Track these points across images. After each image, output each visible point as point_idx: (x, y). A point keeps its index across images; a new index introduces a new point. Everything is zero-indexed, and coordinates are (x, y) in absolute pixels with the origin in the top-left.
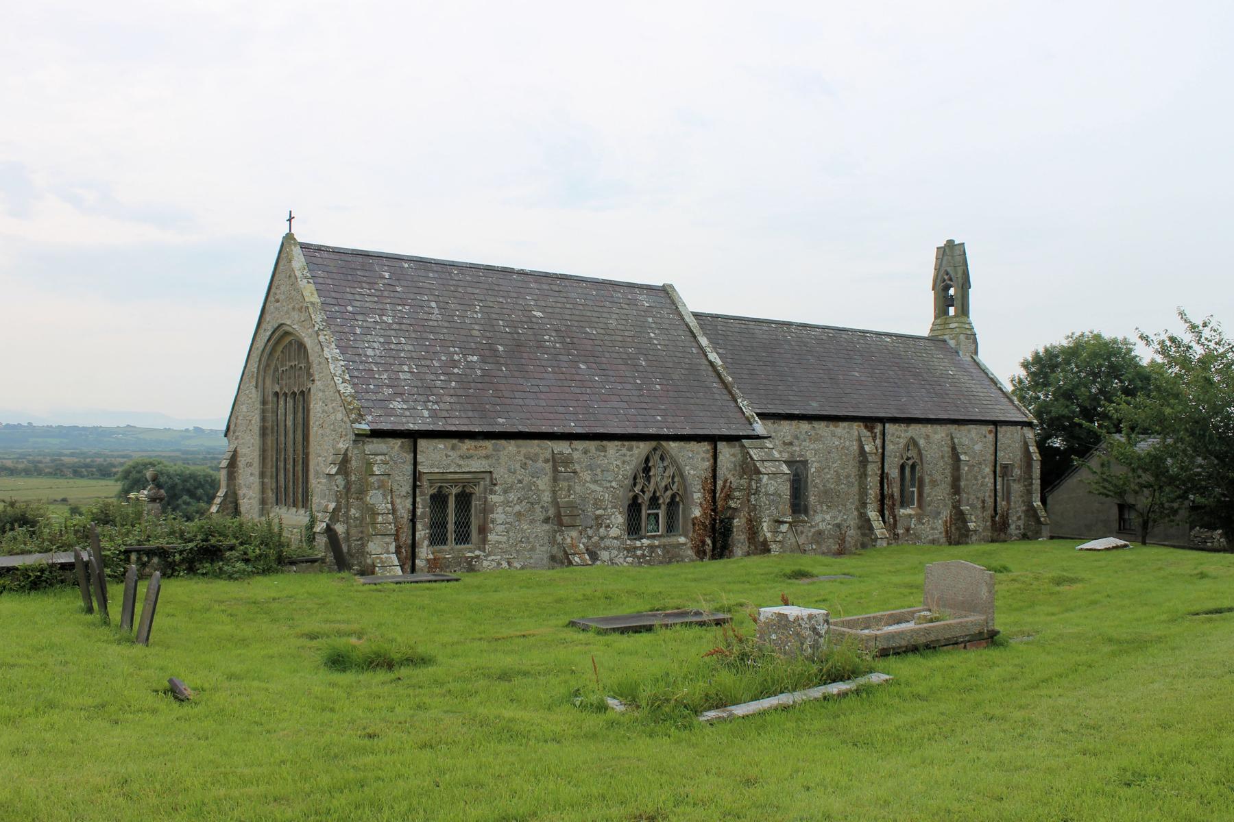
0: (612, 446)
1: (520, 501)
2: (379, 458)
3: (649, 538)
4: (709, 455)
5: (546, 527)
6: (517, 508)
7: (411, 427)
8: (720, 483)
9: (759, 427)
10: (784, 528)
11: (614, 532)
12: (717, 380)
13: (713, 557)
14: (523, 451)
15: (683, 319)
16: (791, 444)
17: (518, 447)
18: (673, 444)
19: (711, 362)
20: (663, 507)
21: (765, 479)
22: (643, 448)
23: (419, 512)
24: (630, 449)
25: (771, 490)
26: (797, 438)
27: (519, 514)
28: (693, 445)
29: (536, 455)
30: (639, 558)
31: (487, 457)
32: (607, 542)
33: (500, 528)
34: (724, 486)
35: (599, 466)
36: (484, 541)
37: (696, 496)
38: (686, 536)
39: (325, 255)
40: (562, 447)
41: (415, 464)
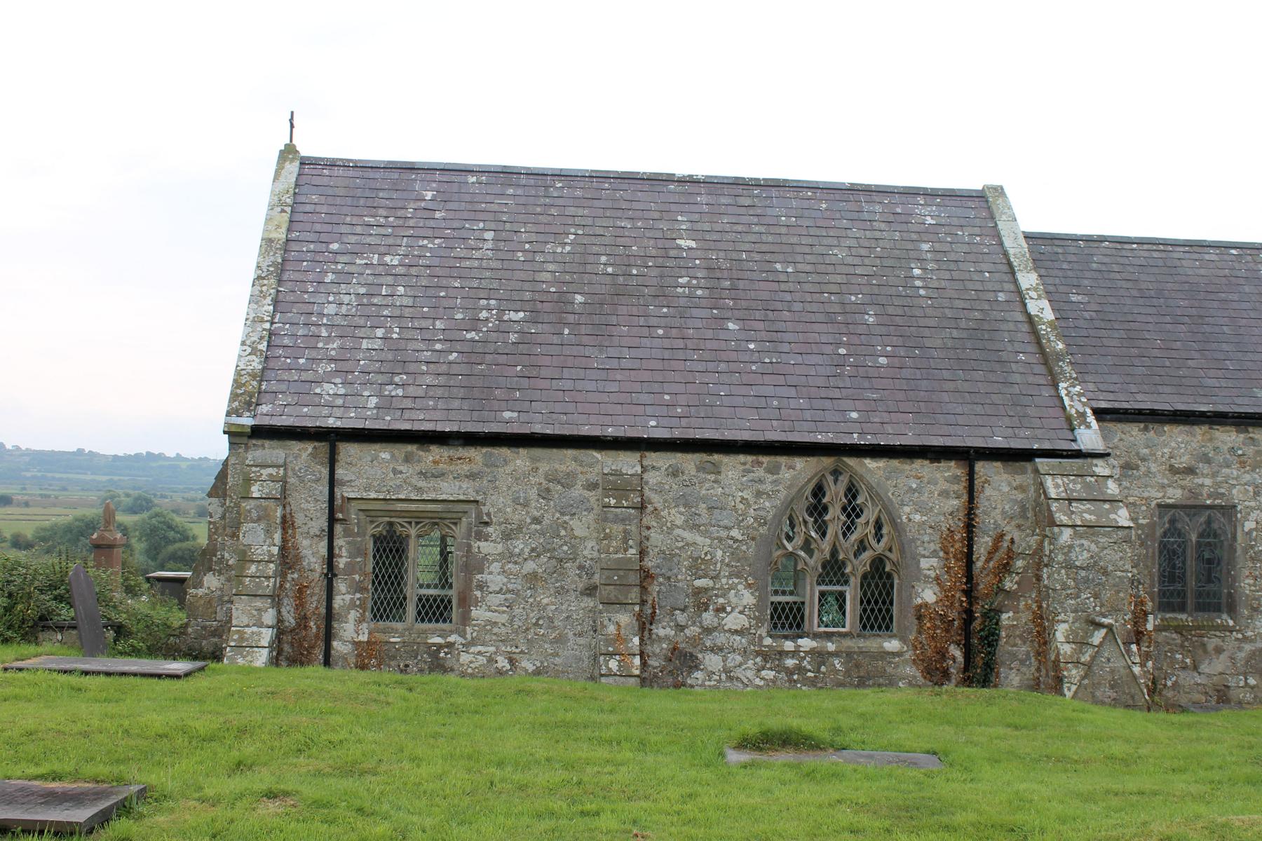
0: (732, 466)
1: (535, 553)
2: (265, 472)
3: (815, 636)
4: (961, 487)
5: (589, 602)
6: (530, 566)
7: (331, 422)
8: (983, 544)
9: (1090, 436)
10: (1098, 636)
11: (734, 620)
12: (1032, 348)
13: (968, 681)
14: (544, 467)
15: (1001, 244)
16: (1190, 471)
17: (533, 460)
18: (870, 463)
19: (1030, 319)
20: (855, 581)
21: (1066, 536)
22: (801, 469)
23: (341, 562)
24: (773, 470)
25: (1082, 558)
26: (1207, 460)
27: (533, 578)
28: (921, 467)
29: (571, 475)
30: (790, 672)
31: (472, 476)
32: (721, 639)
33: (494, 600)
34: (995, 548)
35: (704, 499)
36: (466, 619)
37: (924, 563)
38: (903, 639)
39: (341, 172)
40: (628, 463)
41: (332, 482)
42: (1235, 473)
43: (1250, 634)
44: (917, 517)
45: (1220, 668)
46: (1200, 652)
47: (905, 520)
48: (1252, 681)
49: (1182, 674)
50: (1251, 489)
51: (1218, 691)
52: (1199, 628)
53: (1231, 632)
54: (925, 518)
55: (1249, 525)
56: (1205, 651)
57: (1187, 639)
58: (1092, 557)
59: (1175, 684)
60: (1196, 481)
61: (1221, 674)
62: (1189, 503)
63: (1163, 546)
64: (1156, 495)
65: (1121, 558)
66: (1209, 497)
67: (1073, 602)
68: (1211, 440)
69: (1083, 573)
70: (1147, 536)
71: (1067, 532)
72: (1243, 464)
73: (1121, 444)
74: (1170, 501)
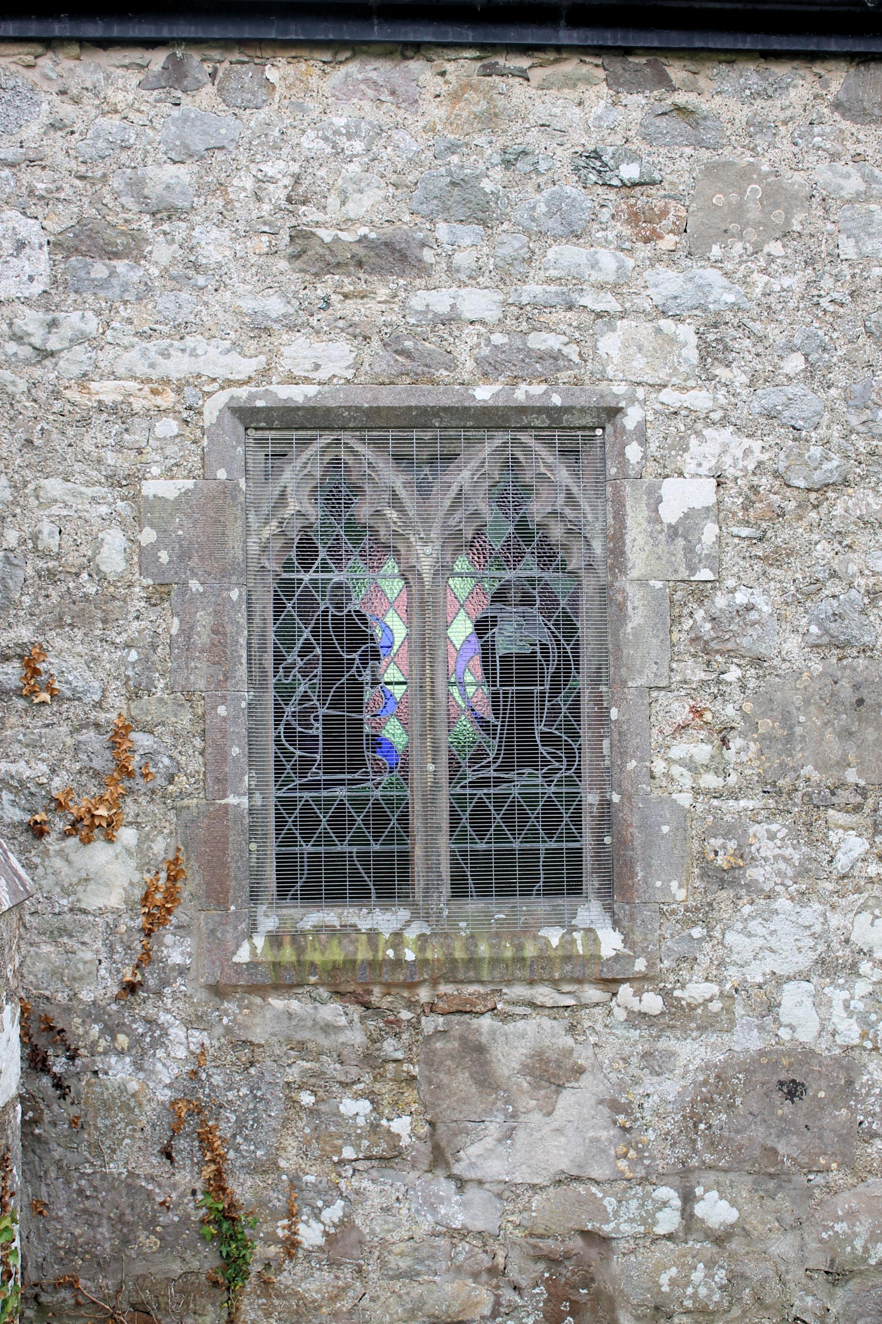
16: (391, 256)
42: (608, 260)
43: (697, 990)
45: (560, 1155)
46: (462, 1082)
48: (715, 1210)
49: (376, 1191)
50: (686, 332)
51: (553, 1261)
52: (450, 970)
53: (611, 983)
55: (682, 496)
56: (486, 1081)
57: (394, 1026)
60: (419, 300)
61: (563, 1180)
62: (388, 398)
64: (224, 367)
66: (488, 369)
68: (490, 119)
70: (183, 555)
72: (644, 224)
73: (55, 146)
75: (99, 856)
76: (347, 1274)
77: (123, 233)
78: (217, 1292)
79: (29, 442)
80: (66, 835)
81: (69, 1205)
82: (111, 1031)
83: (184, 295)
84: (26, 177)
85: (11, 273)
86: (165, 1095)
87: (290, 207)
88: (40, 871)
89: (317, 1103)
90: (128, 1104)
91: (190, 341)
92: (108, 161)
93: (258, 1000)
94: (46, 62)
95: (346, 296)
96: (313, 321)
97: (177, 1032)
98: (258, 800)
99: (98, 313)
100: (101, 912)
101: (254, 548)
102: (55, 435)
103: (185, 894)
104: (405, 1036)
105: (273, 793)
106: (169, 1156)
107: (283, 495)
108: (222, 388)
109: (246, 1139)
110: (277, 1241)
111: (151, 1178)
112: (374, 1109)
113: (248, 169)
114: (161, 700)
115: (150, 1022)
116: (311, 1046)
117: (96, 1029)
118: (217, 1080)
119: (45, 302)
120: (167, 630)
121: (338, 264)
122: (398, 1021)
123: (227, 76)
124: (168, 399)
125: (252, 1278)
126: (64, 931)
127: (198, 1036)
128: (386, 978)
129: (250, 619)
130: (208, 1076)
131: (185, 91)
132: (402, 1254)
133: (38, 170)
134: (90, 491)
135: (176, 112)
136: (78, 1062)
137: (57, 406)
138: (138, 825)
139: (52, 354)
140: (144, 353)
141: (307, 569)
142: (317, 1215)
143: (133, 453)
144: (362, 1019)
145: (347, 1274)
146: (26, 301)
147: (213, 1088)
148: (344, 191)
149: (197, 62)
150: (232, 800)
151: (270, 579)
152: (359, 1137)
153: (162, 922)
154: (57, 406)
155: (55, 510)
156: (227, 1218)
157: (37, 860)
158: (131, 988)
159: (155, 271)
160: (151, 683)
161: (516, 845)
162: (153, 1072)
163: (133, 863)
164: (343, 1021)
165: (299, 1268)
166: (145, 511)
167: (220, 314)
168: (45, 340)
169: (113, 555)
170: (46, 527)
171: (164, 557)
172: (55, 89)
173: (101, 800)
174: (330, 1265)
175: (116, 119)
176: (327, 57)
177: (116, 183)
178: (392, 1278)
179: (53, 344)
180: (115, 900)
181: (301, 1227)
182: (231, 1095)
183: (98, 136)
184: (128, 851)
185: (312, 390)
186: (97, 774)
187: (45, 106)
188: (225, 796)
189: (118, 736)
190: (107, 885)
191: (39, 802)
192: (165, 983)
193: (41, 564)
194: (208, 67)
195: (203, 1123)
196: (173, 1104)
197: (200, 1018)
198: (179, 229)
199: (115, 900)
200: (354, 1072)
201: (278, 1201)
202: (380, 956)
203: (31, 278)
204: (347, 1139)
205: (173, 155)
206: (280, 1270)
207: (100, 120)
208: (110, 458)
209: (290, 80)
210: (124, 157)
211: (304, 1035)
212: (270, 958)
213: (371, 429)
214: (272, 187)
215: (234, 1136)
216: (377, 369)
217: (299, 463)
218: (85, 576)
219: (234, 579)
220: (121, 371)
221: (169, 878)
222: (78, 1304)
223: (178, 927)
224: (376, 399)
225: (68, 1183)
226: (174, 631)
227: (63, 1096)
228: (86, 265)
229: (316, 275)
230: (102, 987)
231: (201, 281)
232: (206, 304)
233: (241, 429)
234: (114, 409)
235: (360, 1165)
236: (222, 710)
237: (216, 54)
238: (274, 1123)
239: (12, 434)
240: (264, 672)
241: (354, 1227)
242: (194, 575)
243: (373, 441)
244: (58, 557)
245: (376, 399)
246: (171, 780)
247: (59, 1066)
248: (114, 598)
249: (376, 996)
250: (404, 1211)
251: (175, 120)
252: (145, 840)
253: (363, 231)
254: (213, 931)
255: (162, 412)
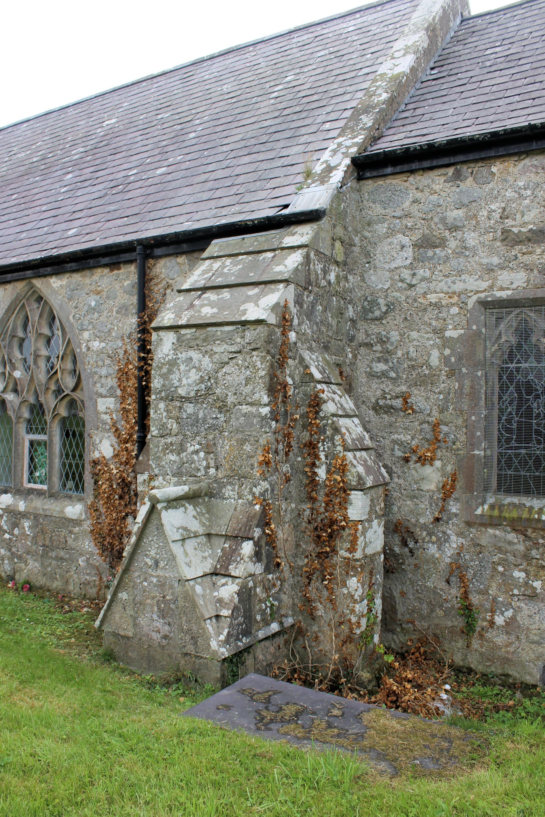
44: (96, 345)
47: (84, 350)
49: (526, 608)
54: (103, 345)
57: (536, 545)
58: (202, 380)
59: (511, 623)
63: (506, 378)
64: (475, 285)
65: (248, 380)
67: (173, 457)
69: (190, 408)
71: (169, 338)
74: (504, 294)
75: (428, 470)
76: (513, 638)
77: (439, 238)
78: (463, 635)
79: (406, 318)
80: (416, 462)
81: (413, 595)
82: (430, 534)
83: (461, 259)
84: (404, 222)
85: (400, 257)
86: (448, 560)
87: (501, 221)
88: (407, 474)
89: (504, 571)
90: (435, 561)
91: (463, 277)
92: (433, 212)
93: (484, 529)
94: (411, 179)
95: (524, 254)
96: (511, 265)
97: (453, 538)
98: (489, 452)
99: (430, 269)
100: (428, 491)
101: (488, 355)
102: (415, 316)
103: (458, 487)
104: (541, 550)
105: (496, 450)
106: (448, 583)
107: (500, 334)
108: (475, 294)
109: (477, 580)
110: (486, 620)
111: (442, 590)
112: (527, 577)
113: (485, 208)
114: (451, 413)
115: (444, 533)
116: (503, 549)
117: (425, 533)
118: (467, 557)
119: (411, 267)
120: (454, 387)
121: (520, 241)
122: (538, 543)
123: (477, 173)
124: (455, 299)
125: (477, 632)
126: (415, 497)
127: (461, 540)
128: (534, 526)
129: (486, 383)
130: (464, 556)
131: (461, 181)
132: (535, 634)
133: (409, 219)
134: (426, 336)
135: (458, 190)
136: (418, 544)
137: (416, 305)
138: (442, 460)
139: (414, 286)
140: (446, 283)
141: (512, 363)
142: (502, 613)
143: (442, 321)
144: (524, 541)
145: (513, 638)
146: (405, 267)
147: (465, 560)
148: (523, 212)
149: (465, 169)
150: (477, 452)
151: (495, 367)
152: (520, 586)
153: (450, 496)
154: (416, 305)
155: (415, 343)
156: (467, 609)
157: (406, 470)
158: (437, 520)
159: (450, 251)
160: (448, 407)
161: (522, 473)
162: (444, 551)
163: (439, 474)
164: (516, 541)
165: (494, 632)
166: (446, 342)
167: (475, 266)
168: (411, 281)
169: (435, 359)
170: (412, 349)
171: (453, 359)
172: (415, 187)
173: (429, 450)
174: (507, 633)
175: (436, 196)
176: (516, 158)
177: (436, 220)
178: (531, 643)
179: (414, 282)
180: (433, 487)
181: (496, 617)
182: (472, 563)
183: (429, 203)
184: (438, 469)
185: (509, 292)
186: (428, 440)
187: (411, 195)
188: (473, 451)
189: (435, 426)
190: (430, 481)
191: (407, 450)
192: (450, 519)
193: (409, 363)
194: (470, 170)
195: (461, 572)
196: (451, 564)
197: (462, 533)
198: (459, 234)
199: (433, 487)
200: (519, 561)
201: (488, 606)
202: (532, 517)
203: (406, 259)
204: (516, 587)
205: (457, 206)
206: (487, 631)
207: (430, 197)
208: (434, 323)
209: (501, 170)
210: (439, 210)
211: (502, 544)
212: (489, 514)
213: (535, 306)
214: (494, 214)
215: (472, 579)
216: (536, 282)
217: (506, 321)
218: (425, 367)
219: (479, 367)
220: (438, 290)
221: (452, 480)
222: (415, 630)
223: (455, 499)
224: (535, 294)
225: (413, 587)
226: (456, 388)
227: (412, 556)
228: (425, 252)
229: (512, 246)
230: (426, 519)
231: (467, 253)
232: (469, 262)
233: (483, 309)
234: (436, 304)
235: (521, 597)
236: (473, 418)
237: (472, 165)
238: (487, 576)
239: (400, 316)
240: (493, 404)
241: (517, 621)
242: (464, 366)
243: (536, 311)
244: (415, 360)
245: (535, 294)
246: (454, 443)
247: (411, 545)
248: (435, 375)
249: (529, 532)
250: (537, 618)
251: (457, 193)
252: (444, 465)
253: (531, 226)
254: (467, 502)
255: (453, 305)
